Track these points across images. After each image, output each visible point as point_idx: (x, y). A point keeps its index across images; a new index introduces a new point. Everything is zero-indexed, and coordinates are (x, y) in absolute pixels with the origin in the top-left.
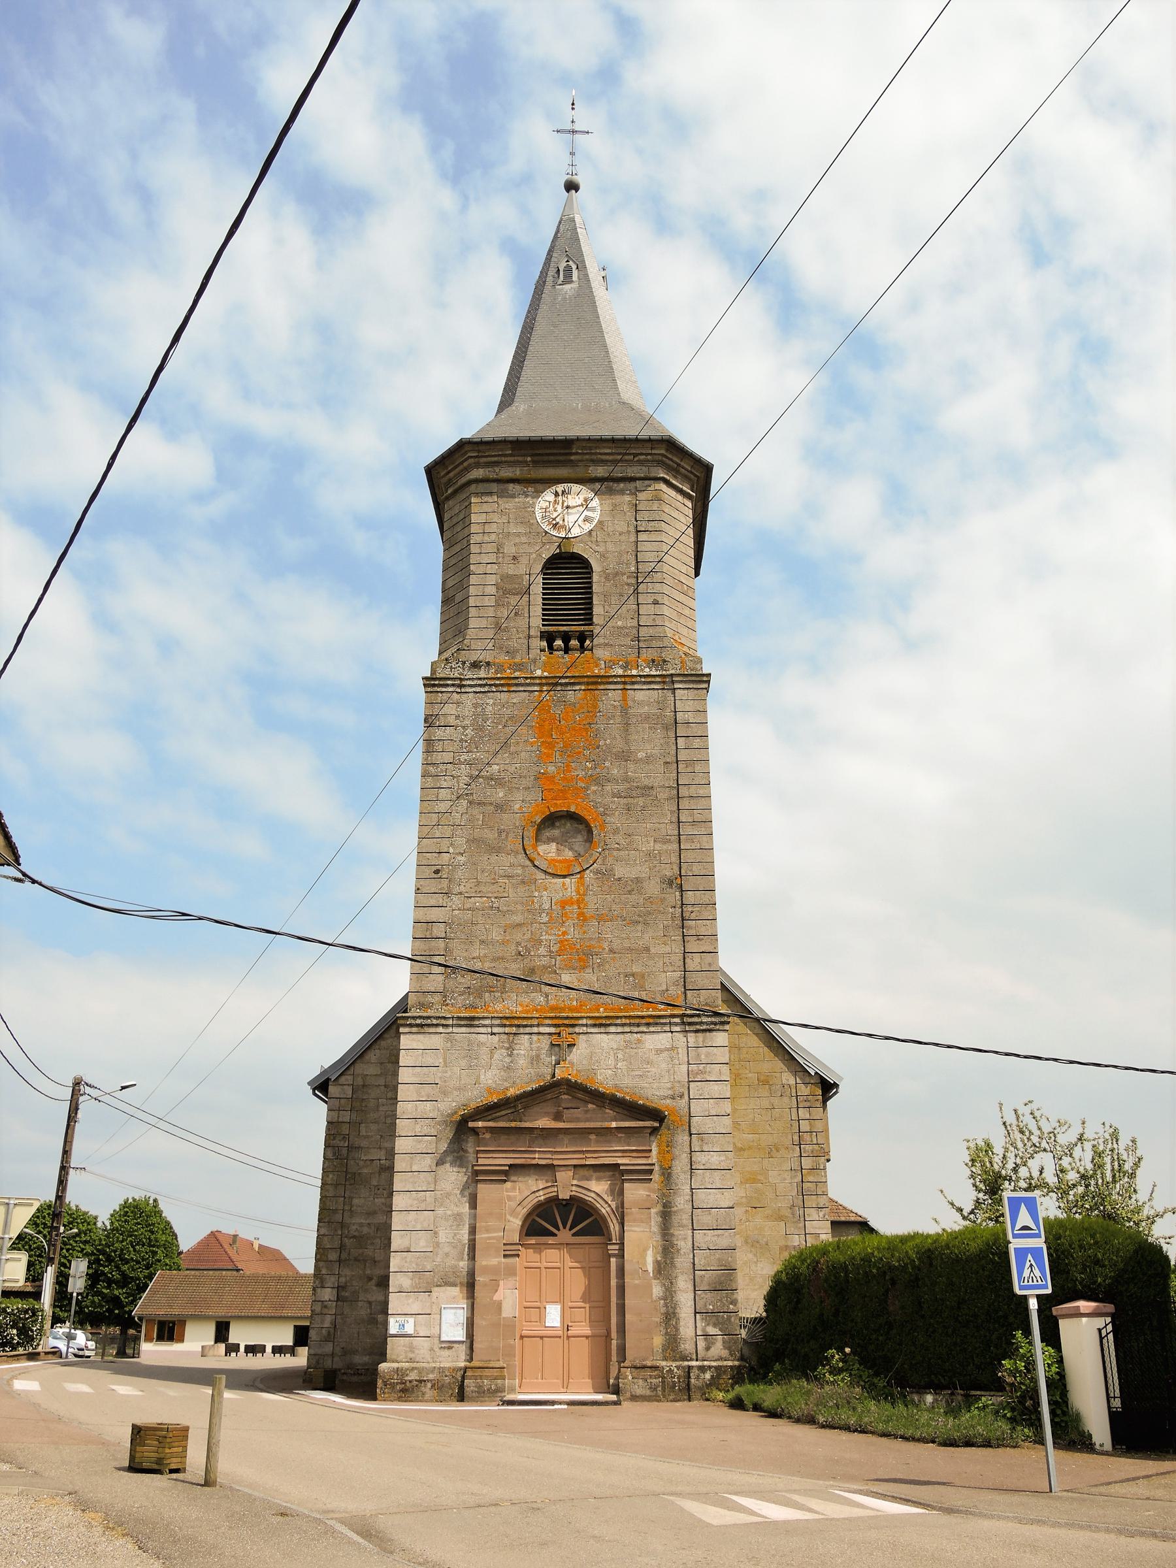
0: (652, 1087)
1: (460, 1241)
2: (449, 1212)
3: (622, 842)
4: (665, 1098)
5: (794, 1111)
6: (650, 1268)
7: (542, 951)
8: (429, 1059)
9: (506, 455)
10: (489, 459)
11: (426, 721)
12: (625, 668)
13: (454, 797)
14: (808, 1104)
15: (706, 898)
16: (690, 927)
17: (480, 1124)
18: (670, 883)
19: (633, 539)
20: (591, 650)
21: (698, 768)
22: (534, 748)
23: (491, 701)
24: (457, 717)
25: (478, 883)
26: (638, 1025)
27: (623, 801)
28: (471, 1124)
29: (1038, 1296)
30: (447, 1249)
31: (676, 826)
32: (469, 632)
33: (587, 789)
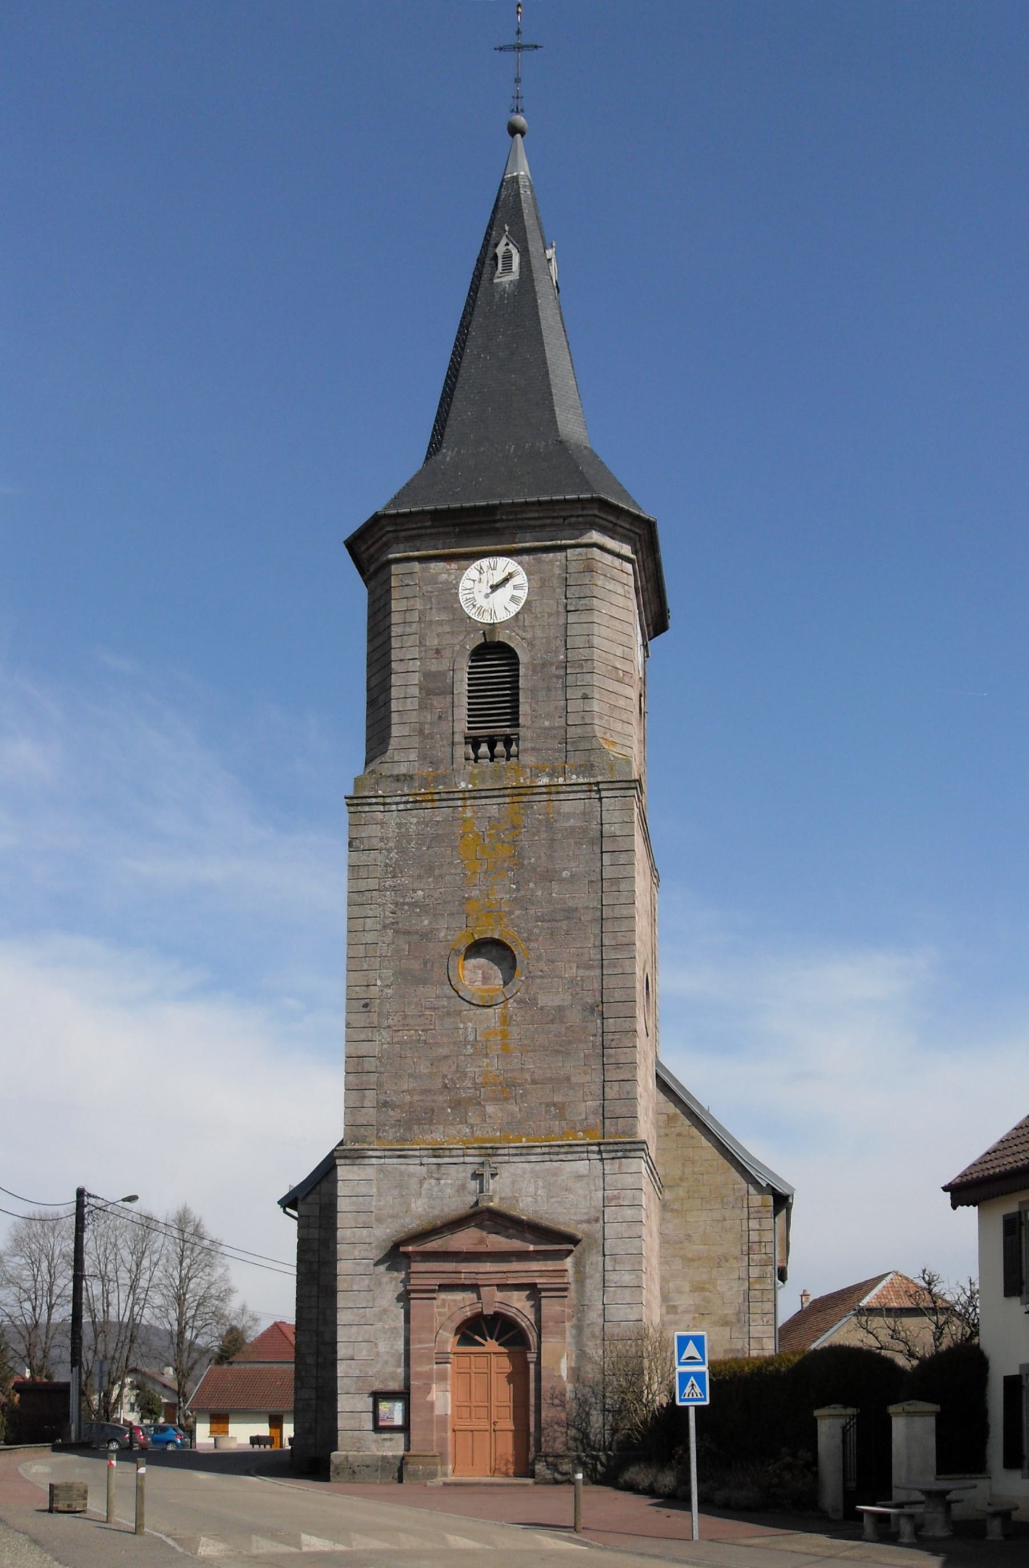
0: (563, 1212)
1: (397, 1351)
2: (387, 1327)
3: (546, 968)
4: (582, 1222)
5: (745, 1222)
6: (564, 1373)
7: (468, 1083)
8: (363, 1189)
9: (426, 528)
10: (409, 533)
11: (350, 845)
12: (551, 775)
13: (379, 927)
14: (759, 1215)
15: (627, 1025)
16: (610, 1056)
17: (410, 1249)
18: (592, 1011)
19: (562, 621)
20: (517, 756)
21: (622, 887)
22: (459, 871)
23: (415, 820)
24: (382, 839)
25: (405, 1017)
26: (558, 1154)
27: (546, 925)
28: (402, 1249)
29: (697, 1407)
30: (385, 1358)
31: (598, 950)
32: (393, 741)
33: (511, 913)
